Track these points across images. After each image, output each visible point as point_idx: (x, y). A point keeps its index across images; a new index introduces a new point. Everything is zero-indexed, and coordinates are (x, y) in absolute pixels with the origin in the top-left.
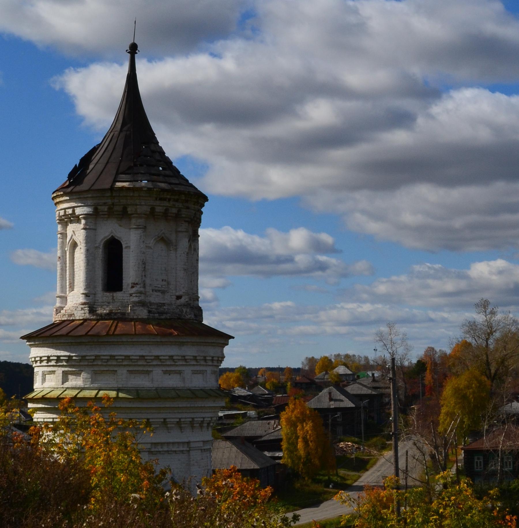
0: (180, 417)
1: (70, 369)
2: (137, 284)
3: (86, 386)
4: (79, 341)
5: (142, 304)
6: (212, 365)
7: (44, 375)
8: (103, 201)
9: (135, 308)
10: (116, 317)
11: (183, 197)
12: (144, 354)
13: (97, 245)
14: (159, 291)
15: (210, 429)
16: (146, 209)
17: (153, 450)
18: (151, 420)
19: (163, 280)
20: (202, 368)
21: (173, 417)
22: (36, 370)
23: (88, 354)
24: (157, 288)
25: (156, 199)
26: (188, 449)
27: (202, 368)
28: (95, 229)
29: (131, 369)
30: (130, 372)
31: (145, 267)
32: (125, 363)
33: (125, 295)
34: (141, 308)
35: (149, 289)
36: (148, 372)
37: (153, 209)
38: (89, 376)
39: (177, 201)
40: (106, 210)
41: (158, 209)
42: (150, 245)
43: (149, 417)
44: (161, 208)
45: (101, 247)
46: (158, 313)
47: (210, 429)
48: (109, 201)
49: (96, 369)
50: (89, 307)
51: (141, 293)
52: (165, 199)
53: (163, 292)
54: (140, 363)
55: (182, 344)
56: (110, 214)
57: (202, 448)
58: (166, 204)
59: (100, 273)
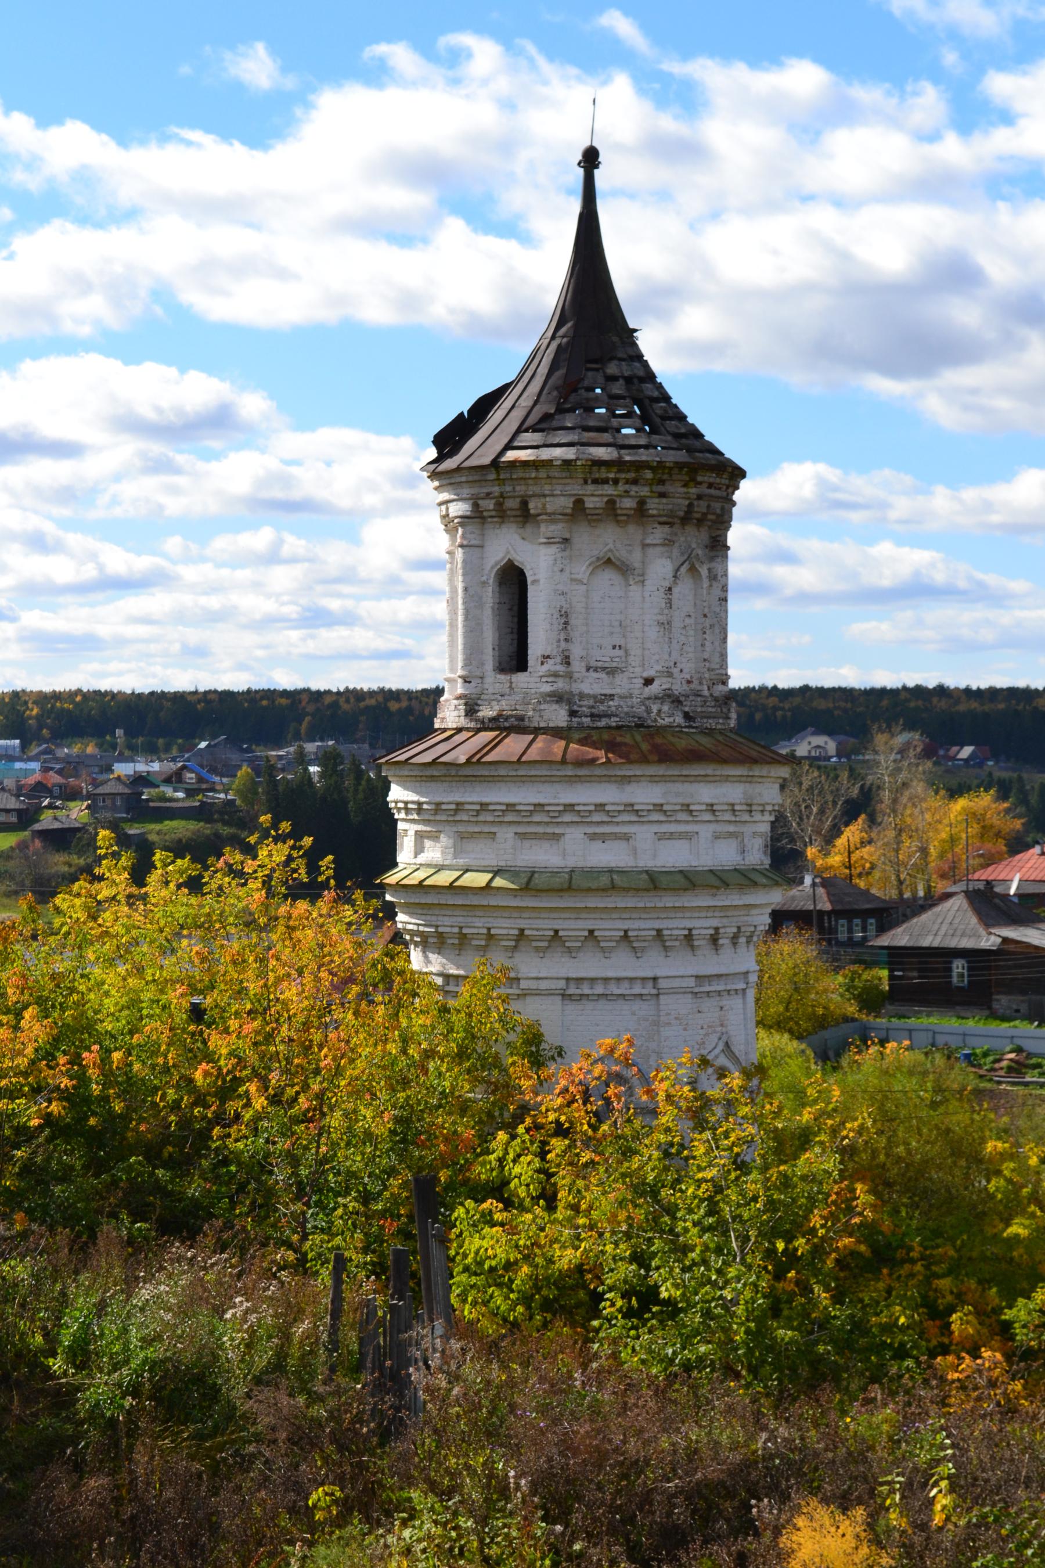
0: (626, 927)
1: (424, 828)
2: (548, 657)
3: (447, 862)
4: (428, 773)
5: (558, 697)
6: (717, 821)
7: (420, 836)
8: (485, 490)
9: (542, 707)
10: (507, 724)
11: (648, 474)
12: (542, 801)
13: (484, 578)
14: (604, 669)
15: (752, 947)
16: (565, 503)
17: (570, 991)
18: (561, 933)
19: (614, 647)
20: (682, 828)
21: (609, 928)
22: (401, 826)
23: (445, 800)
24: (599, 664)
25: (586, 482)
26: (654, 992)
27: (682, 828)
28: (482, 547)
29: (521, 829)
30: (522, 836)
31: (566, 623)
32: (509, 818)
33: (532, 679)
34: (555, 706)
35: (577, 666)
36: (556, 837)
37: (579, 503)
38: (451, 841)
39: (635, 482)
40: (491, 507)
41: (590, 503)
42: (579, 577)
43: (557, 927)
44: (596, 499)
45: (491, 581)
46: (592, 715)
47: (752, 947)
48: (496, 490)
49: (461, 828)
50: (466, 704)
51: (556, 675)
52: (605, 481)
53: (611, 672)
54: (537, 818)
55: (626, 780)
56: (502, 515)
57: (696, 990)
58: (609, 490)
59: (489, 636)
